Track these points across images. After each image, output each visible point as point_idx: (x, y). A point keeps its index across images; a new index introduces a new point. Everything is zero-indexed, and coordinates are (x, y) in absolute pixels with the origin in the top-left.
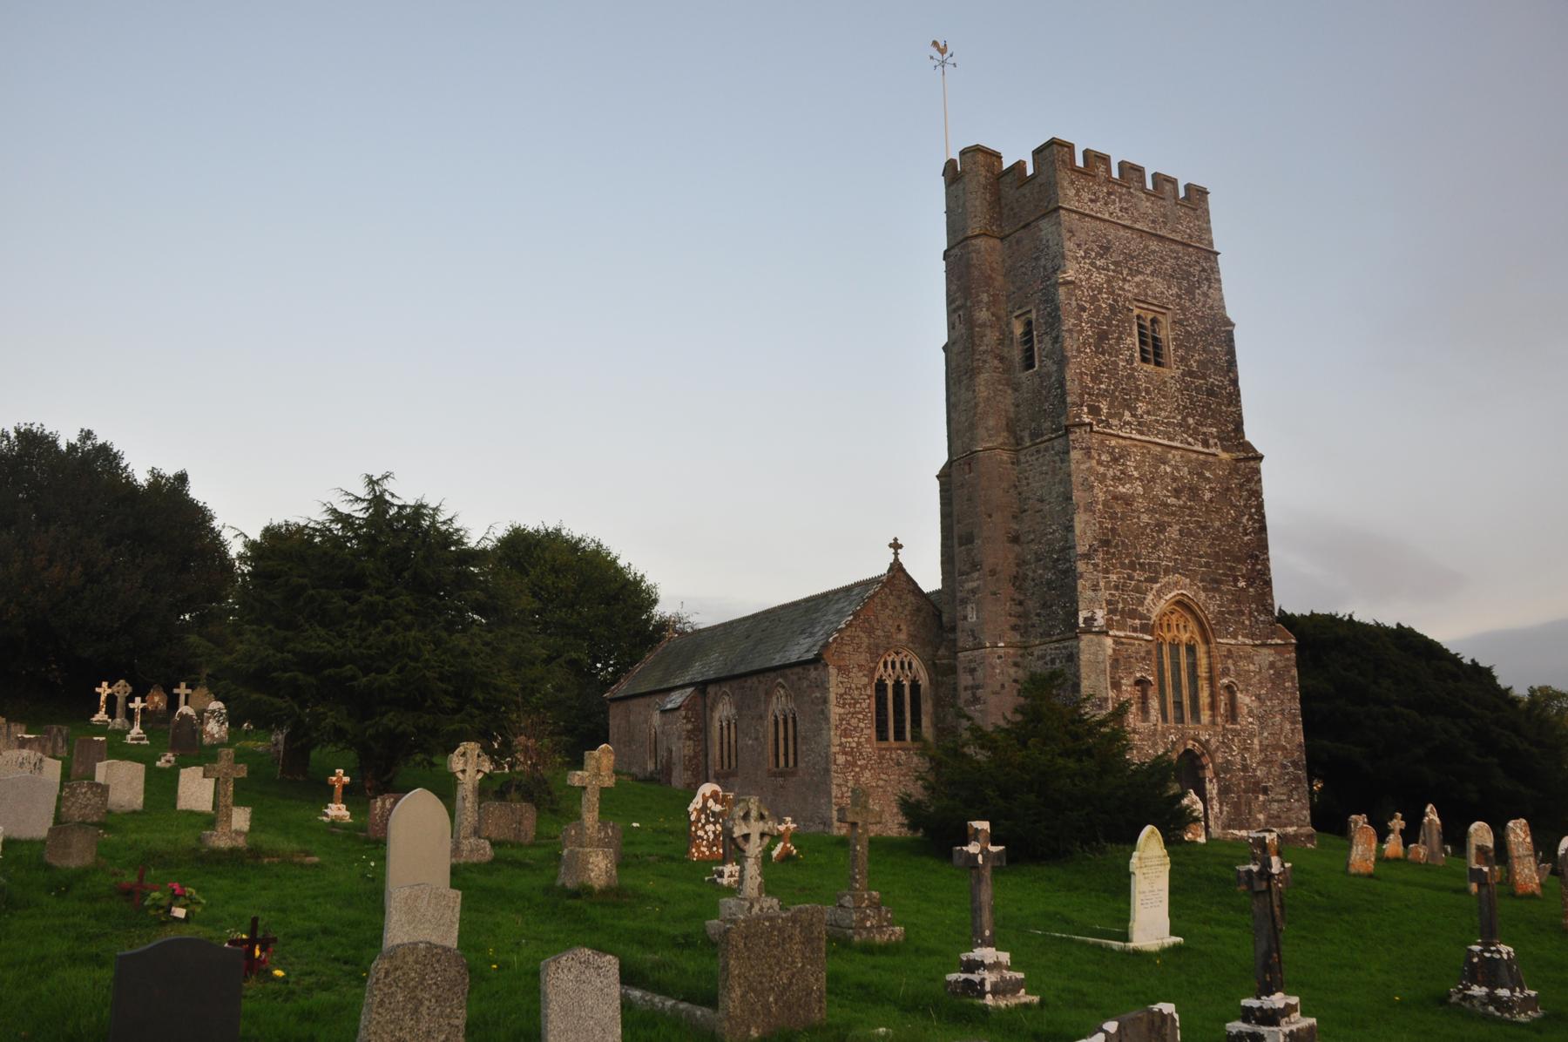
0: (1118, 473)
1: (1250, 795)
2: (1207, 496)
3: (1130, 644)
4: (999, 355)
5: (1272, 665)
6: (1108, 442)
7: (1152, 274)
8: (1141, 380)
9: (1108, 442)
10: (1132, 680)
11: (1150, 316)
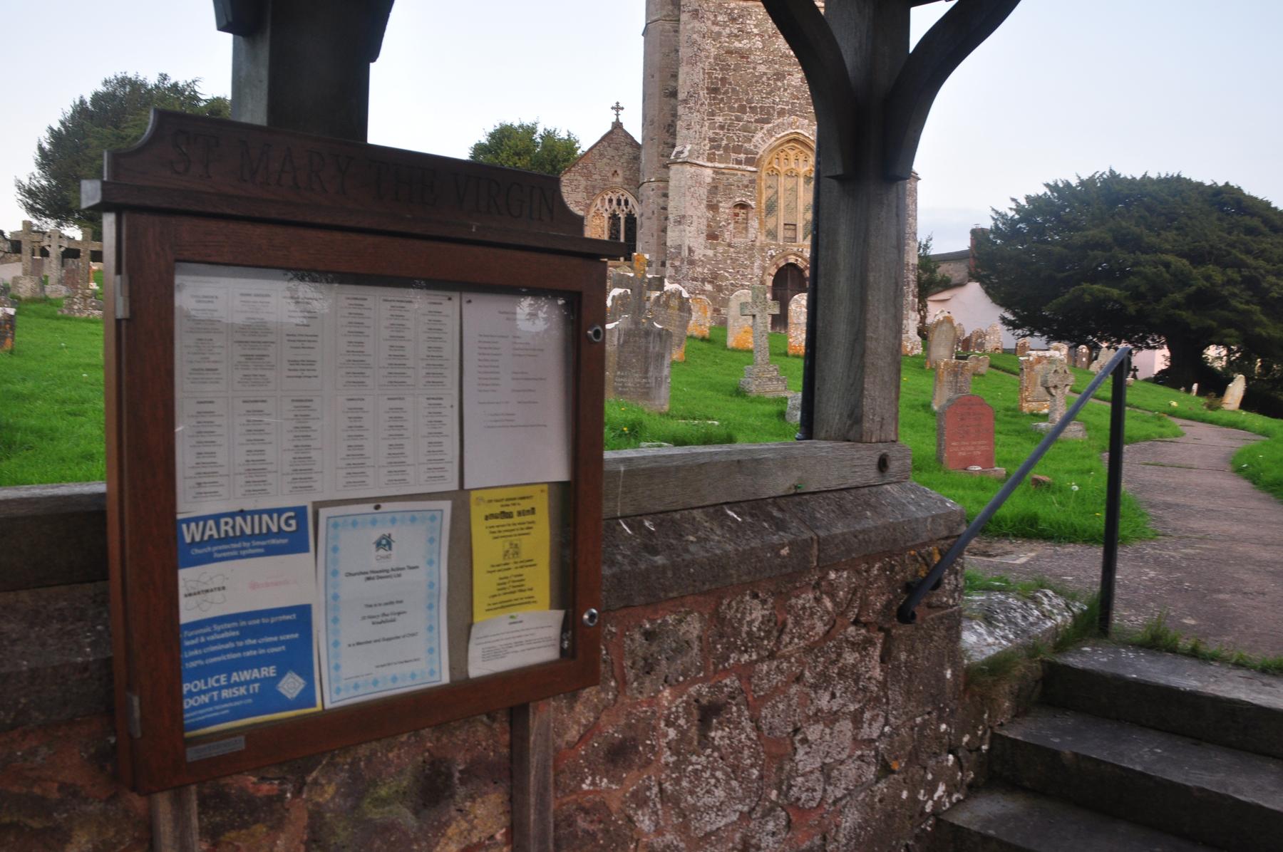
3: (734, 174)
10: (731, 204)
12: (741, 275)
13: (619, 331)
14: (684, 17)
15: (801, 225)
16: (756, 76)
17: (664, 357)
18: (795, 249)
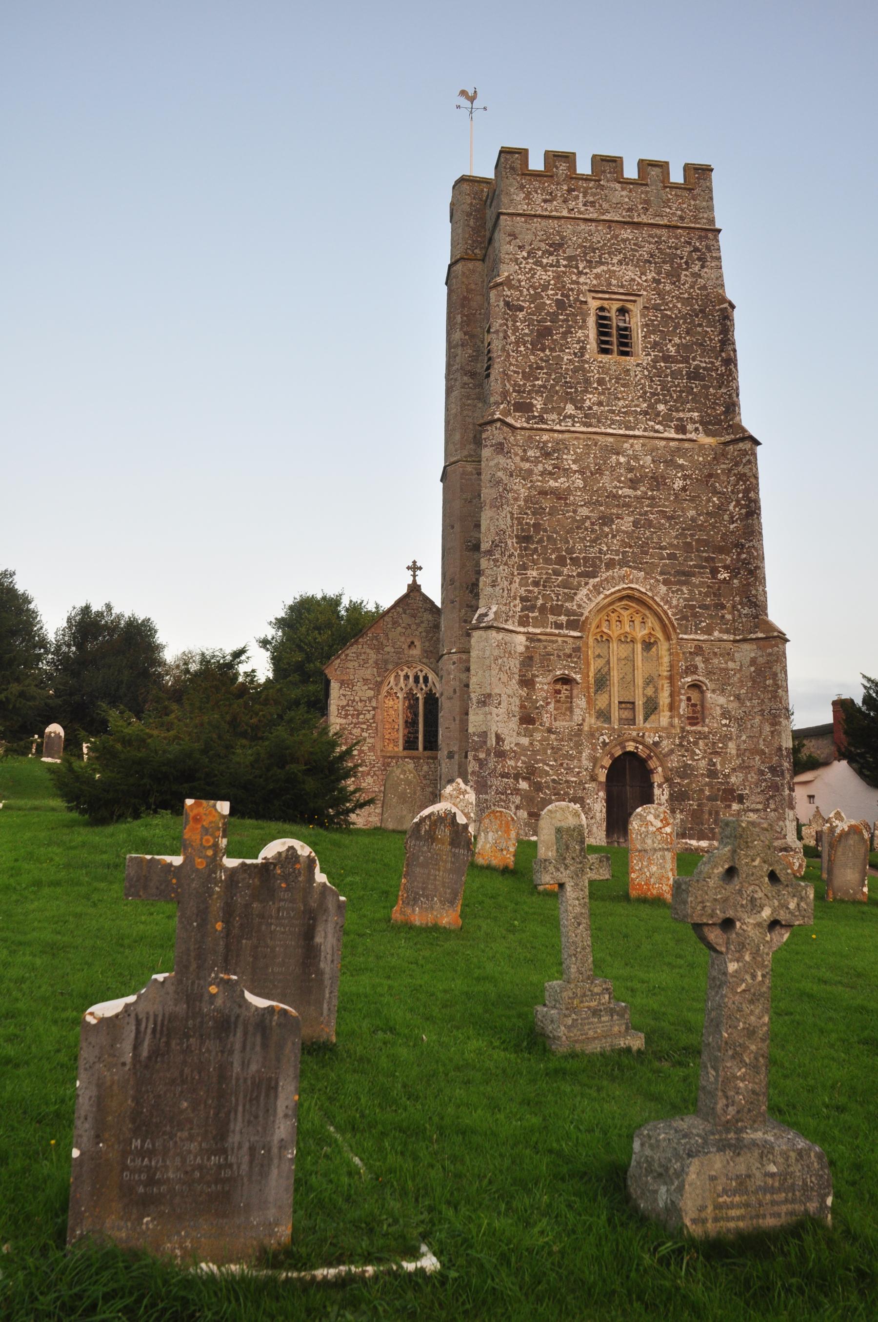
0: (550, 468)
1: (719, 803)
2: (678, 484)
4: (469, 372)
5: (753, 662)
6: (538, 438)
7: (620, 263)
8: (593, 371)
9: (538, 438)
10: (550, 678)
11: (616, 306)
12: (565, 769)
13: (138, 1022)
14: (486, 452)
15: (641, 703)
16: (577, 521)
17: (276, 1088)
18: (634, 734)
